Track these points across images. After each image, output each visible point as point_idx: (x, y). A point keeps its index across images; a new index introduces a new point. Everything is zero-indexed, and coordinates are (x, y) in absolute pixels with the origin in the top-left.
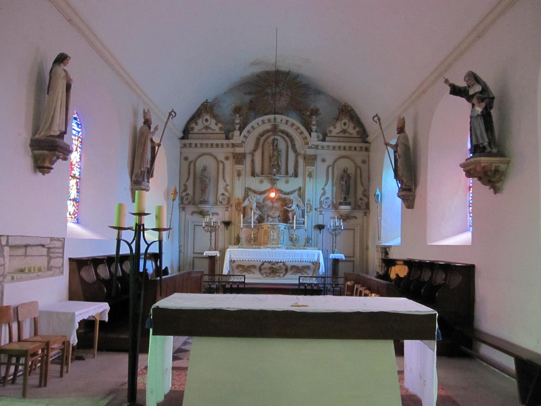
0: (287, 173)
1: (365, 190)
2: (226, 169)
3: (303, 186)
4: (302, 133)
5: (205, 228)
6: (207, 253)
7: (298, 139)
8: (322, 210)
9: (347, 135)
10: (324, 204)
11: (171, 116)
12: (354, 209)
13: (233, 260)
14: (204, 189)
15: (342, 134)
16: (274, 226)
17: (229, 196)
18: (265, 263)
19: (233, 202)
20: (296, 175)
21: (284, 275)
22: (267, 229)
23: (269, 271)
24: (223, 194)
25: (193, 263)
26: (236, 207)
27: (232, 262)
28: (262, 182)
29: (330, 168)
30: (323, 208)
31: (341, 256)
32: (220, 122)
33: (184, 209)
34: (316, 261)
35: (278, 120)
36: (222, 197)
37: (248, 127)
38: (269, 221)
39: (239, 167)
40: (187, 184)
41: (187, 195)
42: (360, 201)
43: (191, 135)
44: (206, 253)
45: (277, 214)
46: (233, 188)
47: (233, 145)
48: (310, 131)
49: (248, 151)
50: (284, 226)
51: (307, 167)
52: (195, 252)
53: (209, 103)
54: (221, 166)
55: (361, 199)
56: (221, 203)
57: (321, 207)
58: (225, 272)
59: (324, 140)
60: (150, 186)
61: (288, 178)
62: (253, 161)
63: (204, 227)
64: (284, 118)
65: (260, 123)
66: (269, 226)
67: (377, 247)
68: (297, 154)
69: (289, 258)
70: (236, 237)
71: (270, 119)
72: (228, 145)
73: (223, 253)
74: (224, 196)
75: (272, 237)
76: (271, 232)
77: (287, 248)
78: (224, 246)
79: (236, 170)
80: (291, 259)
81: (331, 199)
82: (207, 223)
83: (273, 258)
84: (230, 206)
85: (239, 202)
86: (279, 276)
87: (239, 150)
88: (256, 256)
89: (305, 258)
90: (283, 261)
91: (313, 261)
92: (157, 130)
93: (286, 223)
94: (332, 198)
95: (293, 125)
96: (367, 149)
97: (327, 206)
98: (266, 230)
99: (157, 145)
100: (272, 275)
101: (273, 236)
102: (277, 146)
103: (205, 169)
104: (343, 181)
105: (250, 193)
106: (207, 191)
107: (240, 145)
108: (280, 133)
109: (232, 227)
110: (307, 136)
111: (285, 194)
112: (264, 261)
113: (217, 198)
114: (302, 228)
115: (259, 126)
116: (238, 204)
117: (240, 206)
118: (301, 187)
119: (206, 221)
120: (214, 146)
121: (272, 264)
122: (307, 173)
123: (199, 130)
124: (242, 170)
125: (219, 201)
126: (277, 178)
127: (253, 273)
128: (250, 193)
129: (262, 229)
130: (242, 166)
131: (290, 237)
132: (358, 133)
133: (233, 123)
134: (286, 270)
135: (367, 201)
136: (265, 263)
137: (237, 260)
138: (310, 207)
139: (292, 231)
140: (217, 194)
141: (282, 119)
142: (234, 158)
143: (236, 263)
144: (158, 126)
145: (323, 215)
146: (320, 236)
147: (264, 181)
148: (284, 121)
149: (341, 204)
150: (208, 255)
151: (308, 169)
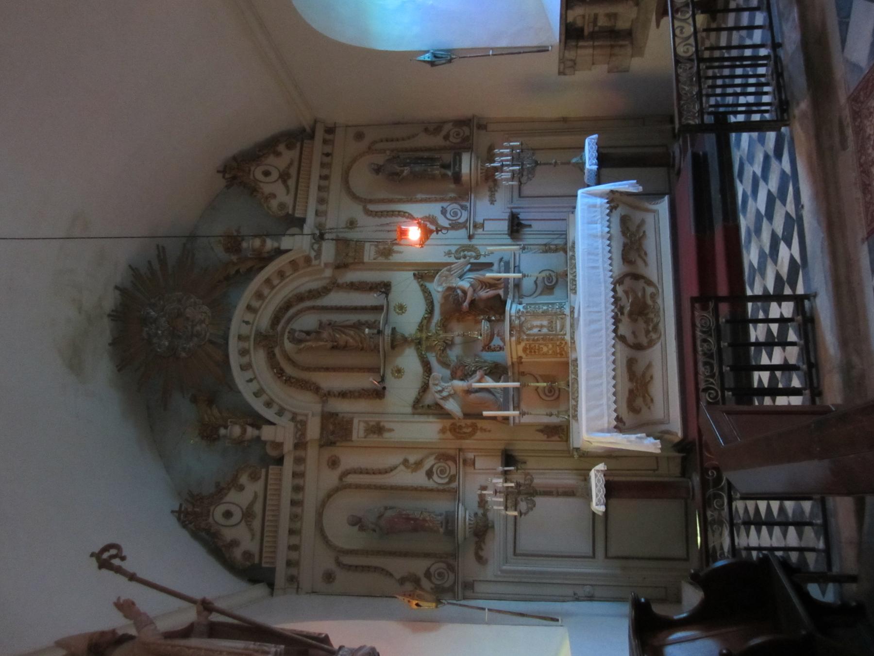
0: (377, 309)
1: (426, 130)
2: (363, 467)
3: (413, 270)
4: (281, 274)
5: (523, 511)
6: (598, 507)
7: (295, 284)
8: (472, 222)
9: (293, 172)
10: (460, 218)
11: (116, 562)
12: (469, 149)
13: (615, 423)
14: (412, 522)
15: (291, 183)
16: (514, 327)
17: (434, 457)
18: (619, 333)
19: (451, 445)
20: (385, 288)
21: (650, 283)
22: (523, 344)
23: (641, 324)
24: (429, 474)
25: (626, 558)
26: (464, 438)
27: (620, 425)
28: (399, 371)
29: (372, 207)
30: (467, 220)
31: (589, 144)
32: (235, 478)
33: (469, 586)
34: (606, 201)
35: (245, 330)
36: (435, 477)
37: (258, 406)
38: (501, 344)
39: (358, 431)
40: (398, 576)
41: (428, 575)
42: (451, 139)
43: (264, 560)
44: (597, 505)
45: (485, 326)
46: (413, 447)
47: (301, 445)
48: (279, 252)
49: (318, 408)
50: (514, 306)
51: (366, 259)
52: (591, 554)
53: (181, 506)
54: (351, 479)
55: (446, 137)
56: (452, 479)
57: (464, 226)
58: (649, 445)
59: (301, 222)
60: (356, 645)
61: (392, 305)
62: (344, 395)
63: (521, 514)
64: (239, 314)
65: (249, 375)
66: (513, 339)
67: (567, 66)
68: (334, 286)
69: (601, 270)
70: (544, 437)
71: (239, 351)
72: (299, 461)
73: (590, 458)
74: (434, 470)
75: (545, 330)
76: (528, 332)
77: (571, 290)
78: (572, 470)
79: (365, 437)
80: (604, 262)
81: (445, 205)
82: (509, 505)
83: (603, 309)
84: (461, 453)
85: (450, 430)
86: (653, 296)
87: (313, 430)
88: (601, 358)
89: (600, 228)
90: (612, 283)
91: (608, 208)
92: (133, 604)
93: (504, 303)
94: (443, 200)
95: (259, 296)
96: (330, 130)
97: (463, 211)
98: (525, 350)
99: (206, 613)
100: (652, 316)
101: (542, 326)
102: (308, 333)
103: (357, 522)
104: (402, 171)
105: (428, 399)
106: (417, 515)
107: (301, 425)
108: (279, 328)
109: (519, 447)
110: (289, 260)
111: (430, 311)
112: (613, 335)
113: (438, 491)
114: (517, 264)
115: (255, 378)
116: (455, 430)
117: (460, 427)
118: (414, 275)
119: (502, 508)
120: (299, 497)
121: (622, 314)
122: (381, 259)
123: (253, 535)
124: (366, 422)
125: (448, 483)
126: (388, 331)
127: (649, 366)
128: (428, 399)
129: (521, 363)
130: (355, 421)
131: (541, 294)
132: (289, 147)
133: (239, 442)
134: (636, 277)
135: (451, 124)
136: (619, 333)
137: (615, 411)
138: (464, 251)
139: (528, 284)
140: (431, 490)
141: (244, 321)
142: (332, 444)
143: (625, 414)
144: (119, 598)
145: (485, 222)
146: (536, 226)
147: (397, 366)
148: (249, 317)
149: (457, 178)
150: (603, 500)
151: (372, 258)
